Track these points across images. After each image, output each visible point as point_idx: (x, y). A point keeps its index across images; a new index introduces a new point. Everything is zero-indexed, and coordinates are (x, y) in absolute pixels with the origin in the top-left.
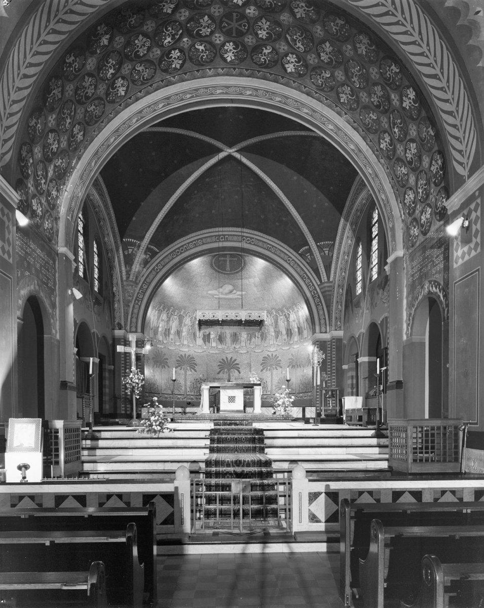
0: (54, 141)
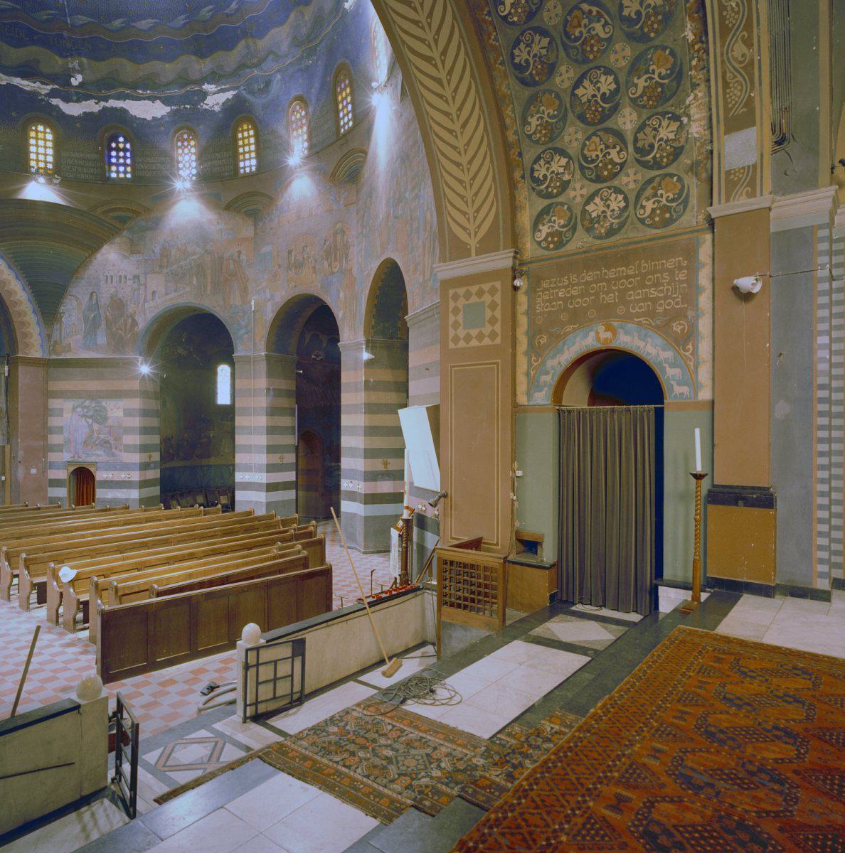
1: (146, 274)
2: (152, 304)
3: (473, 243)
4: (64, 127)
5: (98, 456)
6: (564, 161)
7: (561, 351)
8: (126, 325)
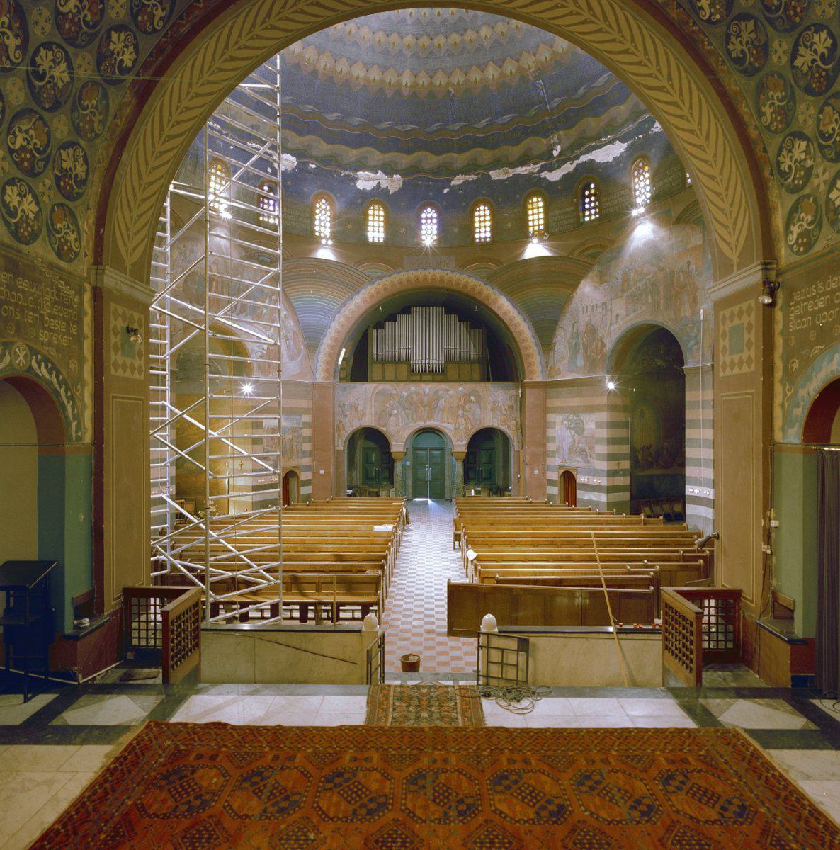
0: (76, 160)
1: (611, 300)
2: (616, 326)
3: (734, 257)
4: (550, 192)
5: (579, 462)
6: (803, 145)
7: (809, 379)
8: (597, 348)
